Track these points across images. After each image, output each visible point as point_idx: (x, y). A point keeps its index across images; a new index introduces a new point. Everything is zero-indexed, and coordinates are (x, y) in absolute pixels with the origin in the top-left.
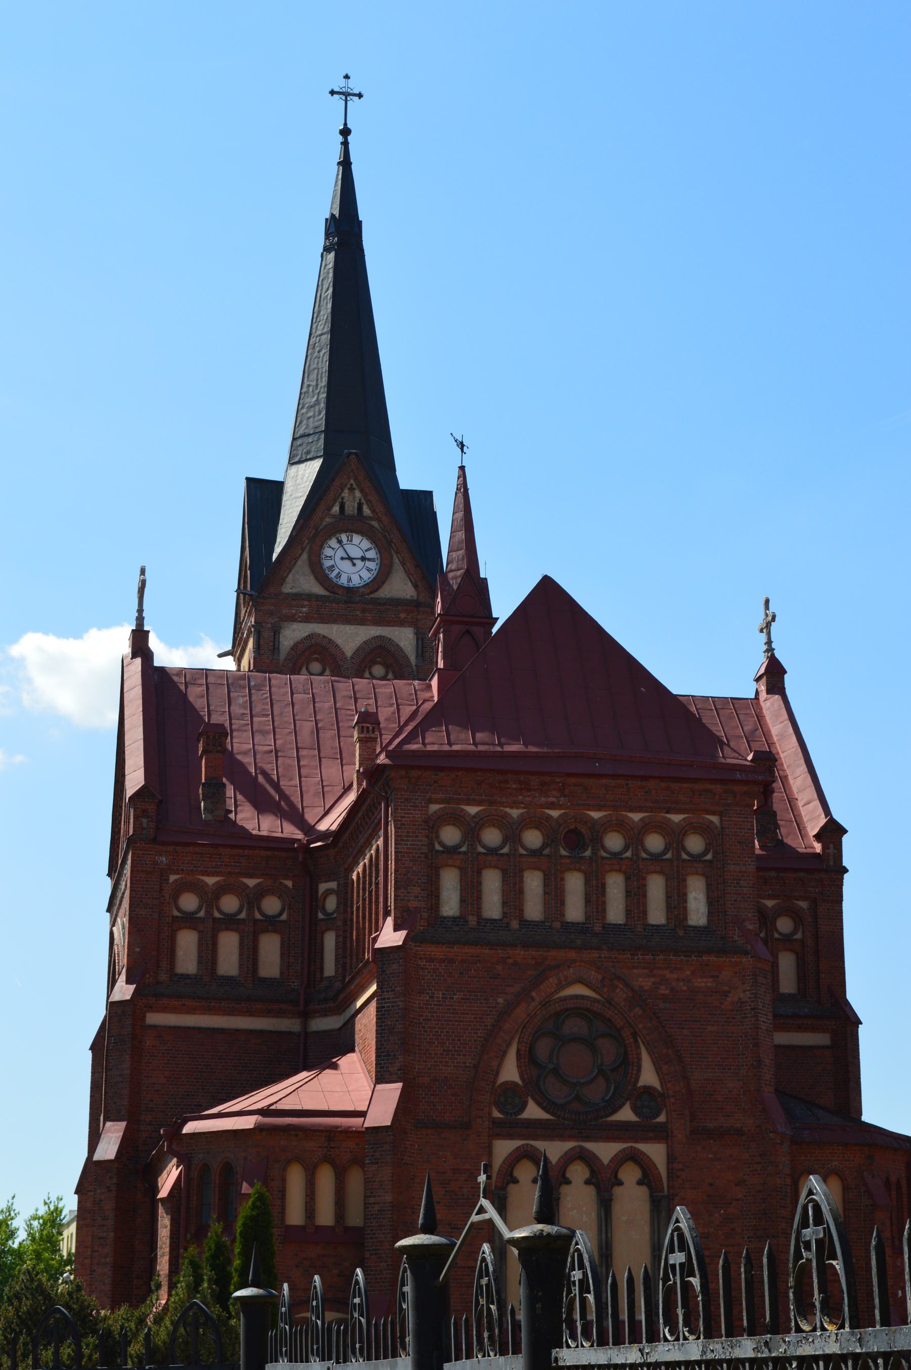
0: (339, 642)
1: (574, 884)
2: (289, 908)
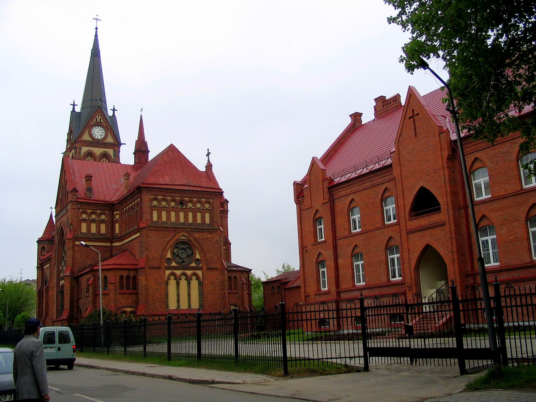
1: (182, 214)
2: (108, 217)
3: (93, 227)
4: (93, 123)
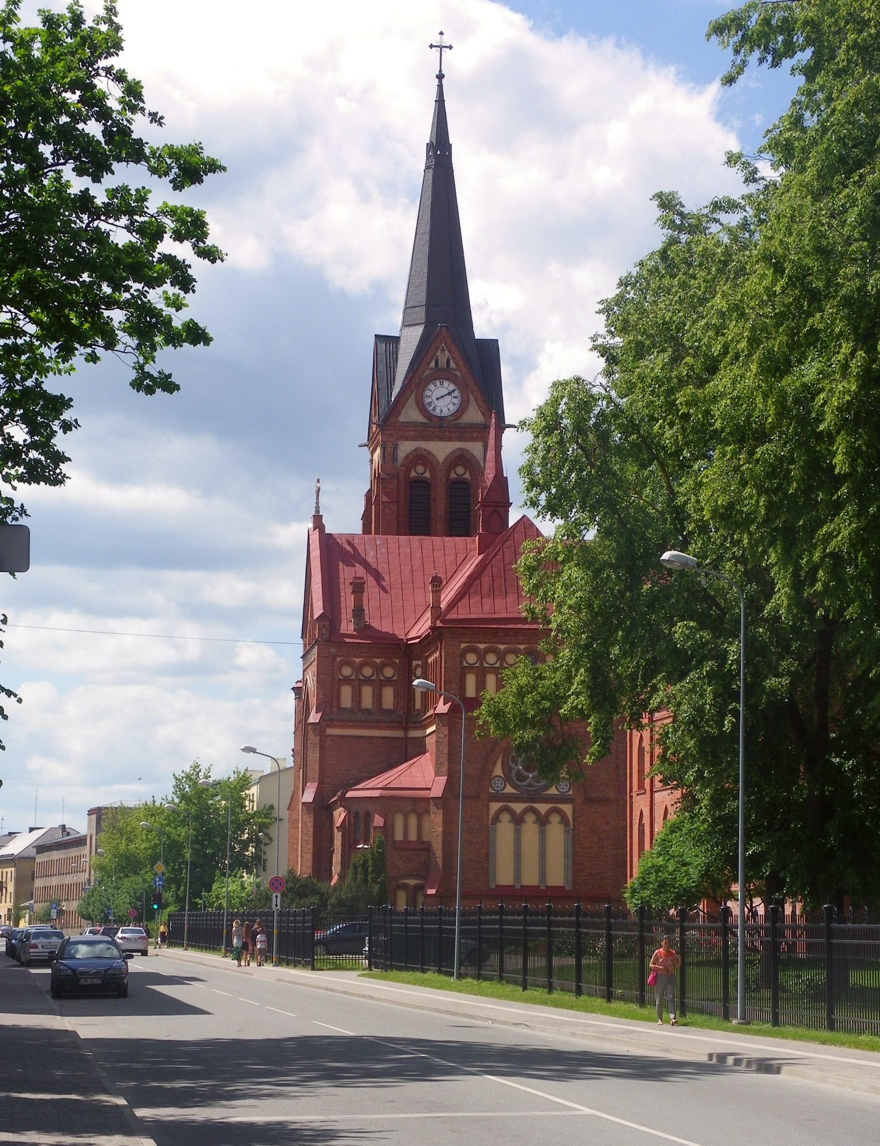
0: (434, 452)
3: (367, 693)
4: (428, 372)
